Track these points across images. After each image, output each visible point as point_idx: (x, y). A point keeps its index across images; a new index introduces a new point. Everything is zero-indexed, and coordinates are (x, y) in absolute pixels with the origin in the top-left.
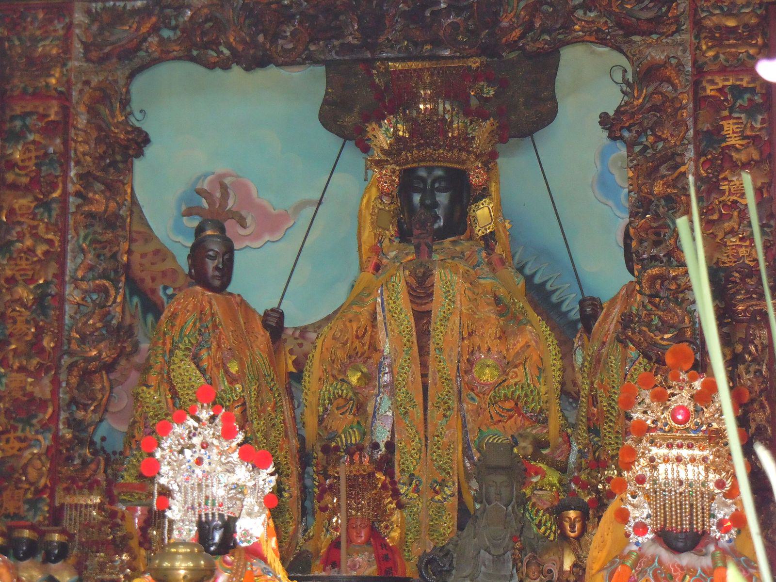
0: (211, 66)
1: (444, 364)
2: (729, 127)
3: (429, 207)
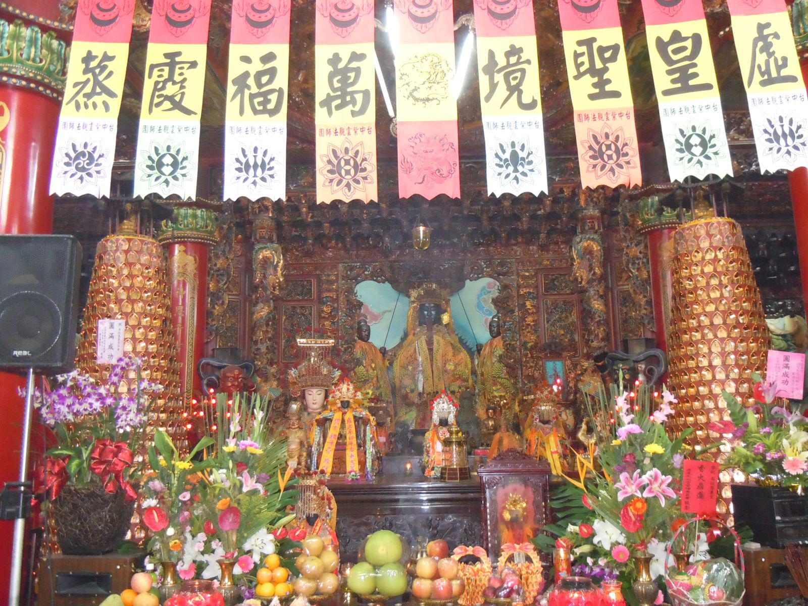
0: (379, 282)
1: (439, 362)
2: (528, 303)
3: (428, 317)
